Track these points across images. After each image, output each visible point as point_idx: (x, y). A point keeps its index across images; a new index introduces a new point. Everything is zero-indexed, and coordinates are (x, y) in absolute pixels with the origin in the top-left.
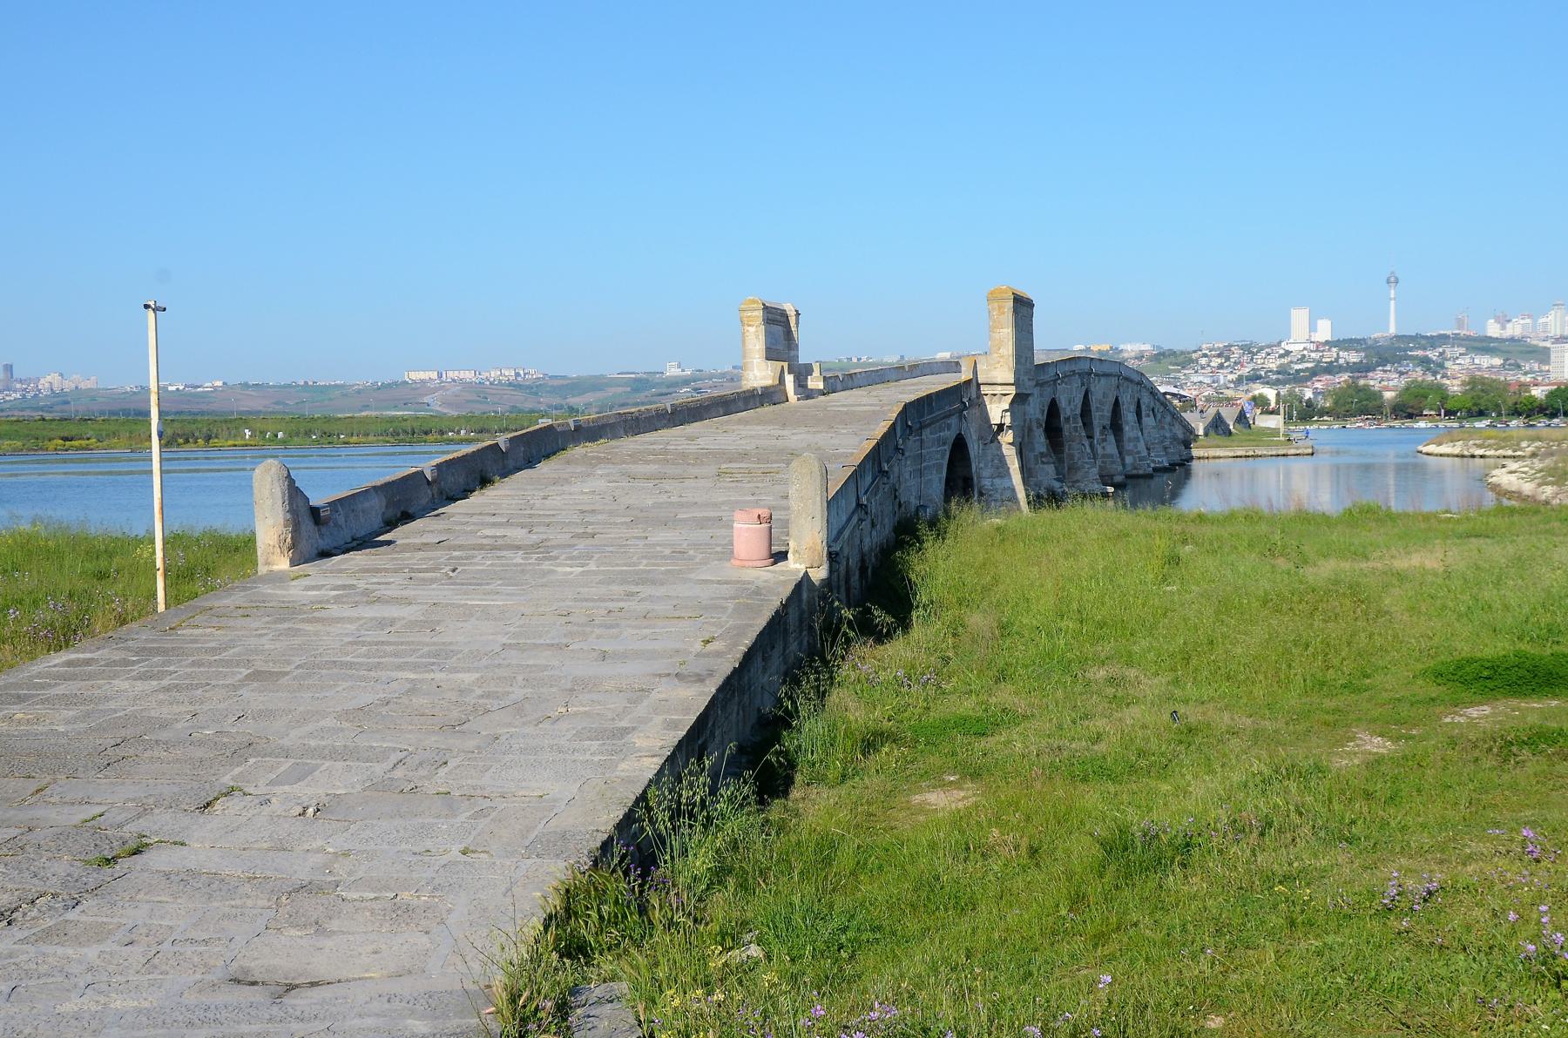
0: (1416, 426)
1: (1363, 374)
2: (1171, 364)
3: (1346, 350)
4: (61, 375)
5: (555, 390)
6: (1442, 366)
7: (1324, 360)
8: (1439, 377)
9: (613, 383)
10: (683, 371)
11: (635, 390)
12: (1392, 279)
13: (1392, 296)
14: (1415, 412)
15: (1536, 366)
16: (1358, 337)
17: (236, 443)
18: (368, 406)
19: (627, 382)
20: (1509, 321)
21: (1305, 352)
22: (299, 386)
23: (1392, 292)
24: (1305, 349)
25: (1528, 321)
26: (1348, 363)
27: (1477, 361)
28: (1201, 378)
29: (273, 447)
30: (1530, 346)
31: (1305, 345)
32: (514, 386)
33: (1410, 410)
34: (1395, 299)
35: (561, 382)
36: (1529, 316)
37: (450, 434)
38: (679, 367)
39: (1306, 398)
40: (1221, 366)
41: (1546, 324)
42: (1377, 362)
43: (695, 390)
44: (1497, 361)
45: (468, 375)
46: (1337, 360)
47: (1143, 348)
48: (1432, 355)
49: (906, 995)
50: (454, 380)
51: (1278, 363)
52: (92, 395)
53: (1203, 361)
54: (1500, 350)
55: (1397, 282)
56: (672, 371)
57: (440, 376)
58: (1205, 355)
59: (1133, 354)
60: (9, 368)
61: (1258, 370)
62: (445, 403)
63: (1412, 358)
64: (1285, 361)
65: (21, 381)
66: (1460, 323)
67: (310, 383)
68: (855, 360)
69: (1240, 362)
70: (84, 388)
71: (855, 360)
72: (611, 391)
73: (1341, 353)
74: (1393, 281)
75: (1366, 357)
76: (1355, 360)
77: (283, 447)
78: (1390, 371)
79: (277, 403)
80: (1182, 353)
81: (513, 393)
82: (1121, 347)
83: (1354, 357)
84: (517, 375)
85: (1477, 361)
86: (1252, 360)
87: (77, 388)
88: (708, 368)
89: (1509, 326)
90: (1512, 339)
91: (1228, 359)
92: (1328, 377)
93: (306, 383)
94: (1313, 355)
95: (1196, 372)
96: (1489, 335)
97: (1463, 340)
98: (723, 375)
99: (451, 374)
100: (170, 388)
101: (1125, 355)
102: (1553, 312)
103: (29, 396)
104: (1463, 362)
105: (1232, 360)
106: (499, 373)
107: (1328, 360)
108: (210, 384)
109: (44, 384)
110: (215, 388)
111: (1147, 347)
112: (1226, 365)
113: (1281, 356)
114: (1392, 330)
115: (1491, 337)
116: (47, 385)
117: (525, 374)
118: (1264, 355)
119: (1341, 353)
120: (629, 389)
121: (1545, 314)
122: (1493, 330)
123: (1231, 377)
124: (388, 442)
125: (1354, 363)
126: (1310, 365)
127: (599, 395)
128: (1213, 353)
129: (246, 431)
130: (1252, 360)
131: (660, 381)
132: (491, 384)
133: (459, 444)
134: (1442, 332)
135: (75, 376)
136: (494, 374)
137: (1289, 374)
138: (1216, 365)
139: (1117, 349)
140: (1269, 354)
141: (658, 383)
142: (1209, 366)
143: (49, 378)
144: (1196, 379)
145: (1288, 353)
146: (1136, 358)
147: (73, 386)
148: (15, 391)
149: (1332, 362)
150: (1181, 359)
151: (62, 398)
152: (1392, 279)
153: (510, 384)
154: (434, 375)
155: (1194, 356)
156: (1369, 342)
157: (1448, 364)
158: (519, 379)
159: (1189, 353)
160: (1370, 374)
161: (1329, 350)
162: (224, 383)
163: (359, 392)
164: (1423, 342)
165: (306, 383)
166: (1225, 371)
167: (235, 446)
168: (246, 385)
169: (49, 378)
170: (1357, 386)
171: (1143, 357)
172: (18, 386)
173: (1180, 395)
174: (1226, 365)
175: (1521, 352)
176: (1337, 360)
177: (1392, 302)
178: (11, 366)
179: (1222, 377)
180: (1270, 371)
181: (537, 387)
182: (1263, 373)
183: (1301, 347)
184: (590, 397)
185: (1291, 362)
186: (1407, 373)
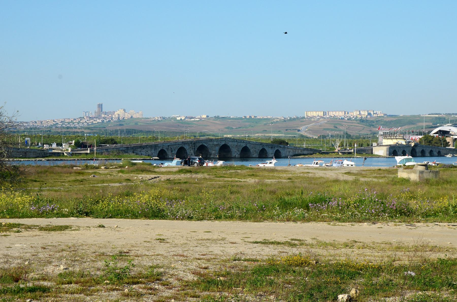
4: (124, 110)
18: (266, 131)
57: (325, 113)
60: (100, 106)
62: (310, 130)
67: (253, 117)
87: (132, 117)
93: (250, 117)
99: (332, 114)
103: (105, 121)
106: (358, 113)
110: (201, 119)
116: (117, 116)
117: (374, 113)
136: (355, 114)
143: (118, 112)
147: (130, 117)
148: (99, 119)
151: (120, 122)
162: (207, 116)
165: (250, 117)
168: (217, 118)
169: (118, 112)
178: (102, 105)
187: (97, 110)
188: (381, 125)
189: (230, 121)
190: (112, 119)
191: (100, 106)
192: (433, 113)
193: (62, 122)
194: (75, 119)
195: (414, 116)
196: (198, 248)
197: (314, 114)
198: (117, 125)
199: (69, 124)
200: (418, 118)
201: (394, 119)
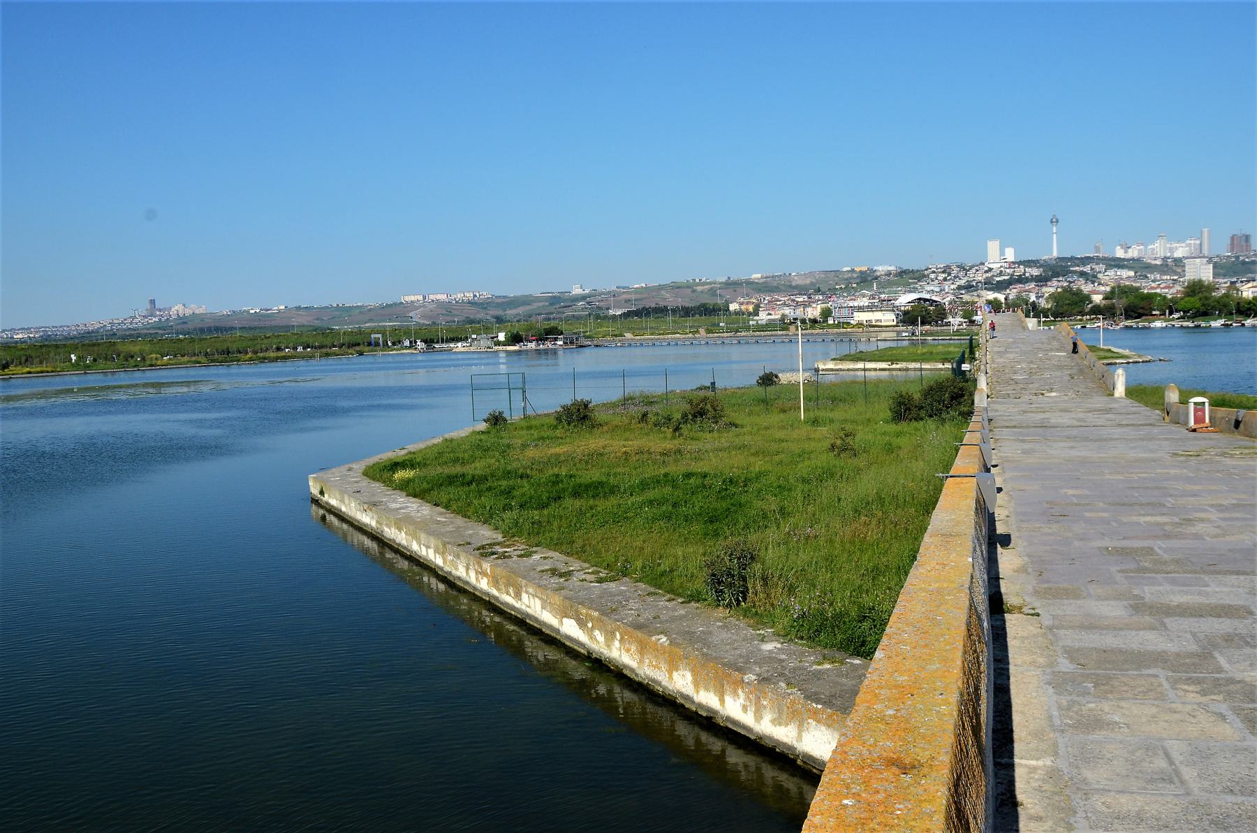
0: (1152, 325)
1: (1044, 283)
2: (910, 278)
3: (1030, 267)
4: (184, 305)
5: (498, 305)
6: (1095, 276)
7: (1015, 274)
8: (1096, 284)
9: (537, 299)
10: (584, 290)
11: (552, 304)
12: (1054, 220)
13: (1055, 231)
14: (1146, 312)
15: (1158, 276)
16: (1033, 259)
17: (32, 370)
18: (372, 320)
19: (547, 299)
20: (1129, 248)
21: (1002, 269)
22: (333, 307)
23: (1055, 228)
24: (1001, 267)
25: (1142, 247)
26: (1032, 276)
27: (1118, 273)
28: (932, 288)
29: (71, 373)
30: (1146, 263)
31: (1001, 264)
32: (472, 304)
33: (1141, 311)
34: (1056, 233)
35: (503, 300)
36: (1142, 244)
37: (287, 350)
38: (581, 288)
39: (1031, 301)
40: (945, 279)
41: (1153, 249)
42: (1052, 275)
43: (588, 303)
44: (1132, 273)
45: (442, 297)
46: (1024, 274)
47: (890, 268)
48: (1087, 269)
49: (843, 426)
50: (433, 301)
51: (984, 276)
52: (201, 317)
53: (933, 276)
54: (1127, 267)
55: (1057, 222)
56: (577, 291)
57: (424, 298)
58: (933, 272)
59: (883, 273)
60: (153, 302)
61: (972, 281)
62: (423, 317)
63: (1075, 272)
64: (989, 275)
65: (160, 310)
66: (1097, 249)
68: (697, 281)
69: (958, 276)
70: (198, 313)
71: (697, 281)
72: (535, 305)
73: (1027, 269)
74: (1054, 221)
75: (1044, 271)
76: (1037, 274)
77: (83, 372)
78: (1062, 281)
79: (317, 319)
80: (918, 271)
81: (469, 308)
82: (875, 268)
83: (1035, 272)
84: (475, 296)
85: (1118, 273)
86: (966, 274)
87: (193, 313)
88: (600, 289)
89: (1130, 250)
90: (1133, 259)
91: (949, 274)
92: (1021, 285)
93: (338, 305)
94: (1008, 271)
95: (928, 284)
96: (1118, 256)
97: (1102, 260)
98: (609, 292)
99: (432, 297)
100: (251, 311)
101: (878, 274)
102: (1158, 241)
103: (163, 319)
104: (1109, 274)
105: (952, 275)
106: (463, 295)
107: (1018, 274)
108: (277, 308)
109: (173, 311)
110: (279, 310)
111: (892, 268)
112: (948, 278)
113: (986, 272)
114: (1055, 254)
115: (1120, 258)
116: (175, 312)
117: (480, 296)
118: (974, 271)
119: (1027, 269)
120: (547, 304)
121: (1153, 243)
122: (1120, 253)
123: (952, 287)
124: (199, 363)
125: (1036, 276)
126: (1007, 277)
127: (528, 308)
128: (939, 270)
129: (72, 356)
130: (966, 274)
131: (567, 298)
132: (457, 302)
133: (273, 361)
134: (1087, 255)
135: (192, 306)
136: (460, 296)
137: (993, 284)
138: (942, 278)
139: (872, 269)
140: (978, 271)
141: (566, 299)
142: (937, 279)
144: (929, 288)
145: (990, 270)
146: (886, 275)
147: (192, 312)
148: (155, 317)
149: (1021, 275)
150: (917, 275)
151: (183, 320)
152: (1054, 220)
153: (469, 302)
154: (420, 298)
155: (926, 272)
156: (1042, 262)
157: (1100, 276)
158: (476, 298)
159: (922, 271)
160: (1049, 283)
161: (1018, 267)
162: (286, 307)
163: (370, 310)
164: (1077, 262)
165: (338, 305)
166: (948, 283)
167: (30, 373)
168: (299, 308)
170: (1071, 289)
171: (891, 274)
172: (158, 313)
173: (932, 300)
174: (948, 278)
175: (1142, 268)
176: (1024, 274)
177: (1055, 235)
178: (154, 300)
179: (946, 287)
180: (979, 282)
181: (487, 303)
182: (974, 284)
183: (999, 265)
184: (520, 310)
185: (994, 276)
186: (1074, 282)
187: (149, 307)
188: (493, 307)
189: (315, 310)
190: (170, 316)
191: (153, 302)
192: (545, 291)
193: (110, 323)
194: (125, 320)
195: (526, 296)
196: (601, 444)
197: (413, 298)
198: (179, 324)
199: (119, 325)
200: (531, 298)
201: (506, 300)
